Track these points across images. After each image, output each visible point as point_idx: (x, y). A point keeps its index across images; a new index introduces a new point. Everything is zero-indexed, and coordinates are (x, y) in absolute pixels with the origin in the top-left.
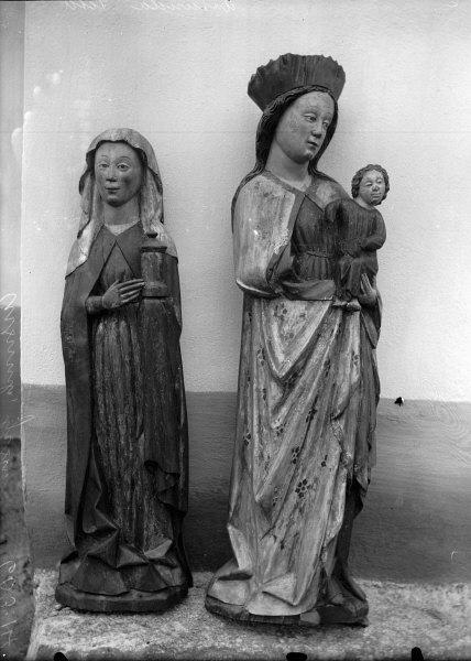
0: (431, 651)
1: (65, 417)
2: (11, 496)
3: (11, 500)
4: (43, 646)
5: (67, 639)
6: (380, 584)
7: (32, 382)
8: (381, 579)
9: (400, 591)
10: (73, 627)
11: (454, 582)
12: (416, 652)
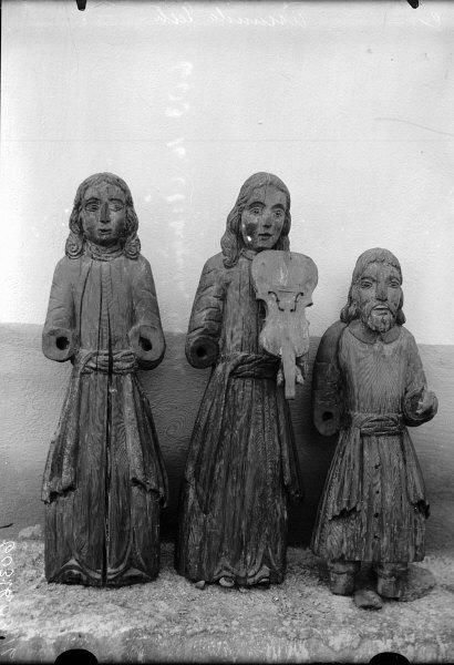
2: (385, 620)
10: (37, 607)
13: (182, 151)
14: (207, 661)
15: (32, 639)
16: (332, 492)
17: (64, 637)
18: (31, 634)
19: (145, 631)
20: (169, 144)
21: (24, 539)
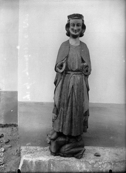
0: (114, 171)
1: (56, 58)
2: (12, 137)
3: (12, 138)
4: (24, 160)
5: (30, 158)
6: (103, 148)
7: (20, 101)
8: (103, 147)
9: (108, 149)
10: (31, 156)
11: (121, 147)
12: (111, 171)
13: (5, 59)
14: (53, 172)
15: (31, 161)
16: (68, 117)
17: (37, 161)
18: (31, 160)
19: (52, 160)
20: (27, 92)
21: (27, 146)
